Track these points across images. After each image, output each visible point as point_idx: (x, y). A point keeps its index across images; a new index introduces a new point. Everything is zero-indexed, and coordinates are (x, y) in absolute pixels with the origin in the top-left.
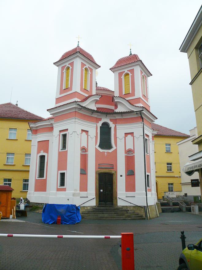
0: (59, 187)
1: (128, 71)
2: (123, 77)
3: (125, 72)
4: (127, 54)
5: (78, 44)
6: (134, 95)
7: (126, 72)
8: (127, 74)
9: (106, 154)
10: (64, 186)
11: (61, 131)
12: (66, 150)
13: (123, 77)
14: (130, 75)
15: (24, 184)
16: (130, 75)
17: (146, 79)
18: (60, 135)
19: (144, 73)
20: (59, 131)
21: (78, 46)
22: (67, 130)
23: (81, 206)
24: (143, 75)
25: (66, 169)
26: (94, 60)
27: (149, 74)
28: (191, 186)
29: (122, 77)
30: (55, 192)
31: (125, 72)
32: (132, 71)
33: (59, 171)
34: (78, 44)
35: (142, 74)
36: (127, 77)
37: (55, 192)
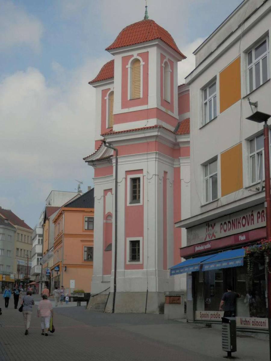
0: (128, 263)
1: (138, 55)
2: (129, 66)
3: (132, 56)
4: (141, 18)
5: (146, 11)
6: (147, 104)
7: (135, 56)
8: (137, 61)
10: (139, 259)
11: (128, 172)
12: (141, 204)
13: (129, 66)
14: (142, 63)
16: (141, 64)
17: (172, 68)
18: (126, 179)
19: (168, 57)
20: (103, 191)
21: (146, 17)
22: (141, 171)
23: (102, 293)
24: (166, 63)
25: (141, 235)
26: (175, 45)
27: (178, 57)
28: (91, 294)
29: (127, 67)
30: (123, 270)
31: (132, 56)
32: (145, 56)
33: (127, 238)
34: (146, 11)
35: (165, 61)
36: (136, 65)
37: (102, 275)
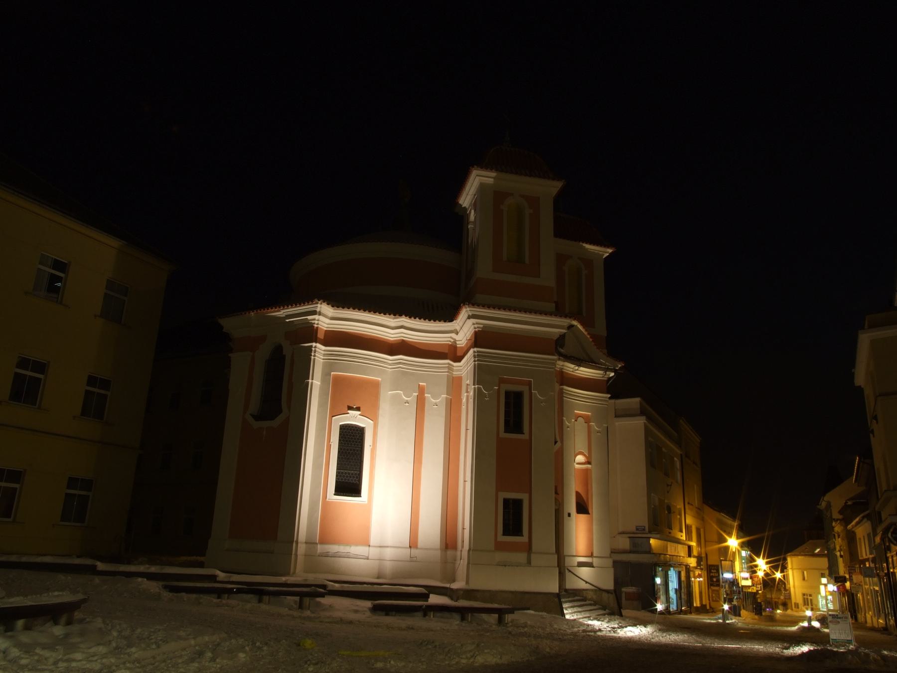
9: (265, 432)
15: (87, 392)
